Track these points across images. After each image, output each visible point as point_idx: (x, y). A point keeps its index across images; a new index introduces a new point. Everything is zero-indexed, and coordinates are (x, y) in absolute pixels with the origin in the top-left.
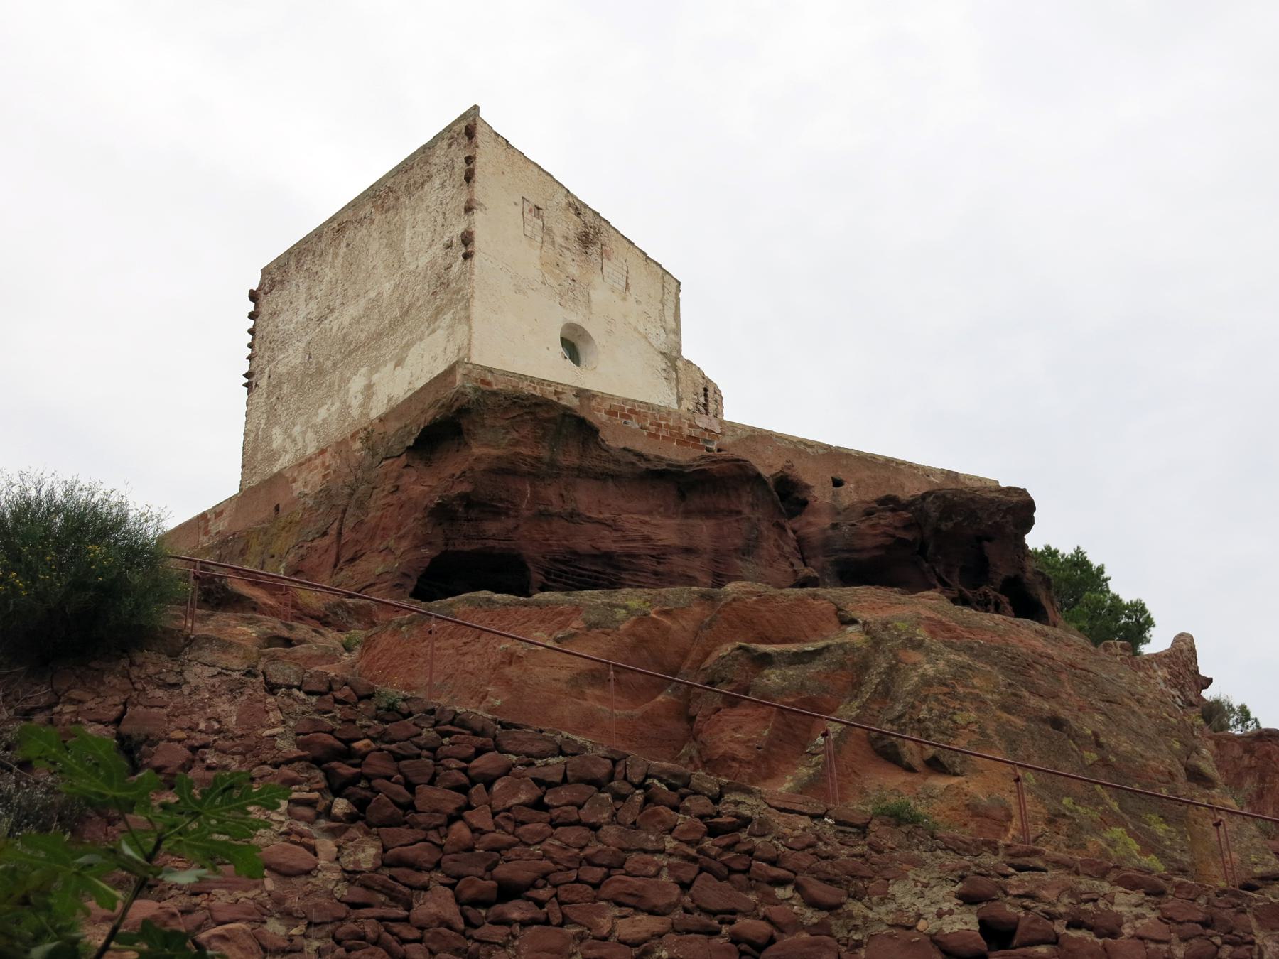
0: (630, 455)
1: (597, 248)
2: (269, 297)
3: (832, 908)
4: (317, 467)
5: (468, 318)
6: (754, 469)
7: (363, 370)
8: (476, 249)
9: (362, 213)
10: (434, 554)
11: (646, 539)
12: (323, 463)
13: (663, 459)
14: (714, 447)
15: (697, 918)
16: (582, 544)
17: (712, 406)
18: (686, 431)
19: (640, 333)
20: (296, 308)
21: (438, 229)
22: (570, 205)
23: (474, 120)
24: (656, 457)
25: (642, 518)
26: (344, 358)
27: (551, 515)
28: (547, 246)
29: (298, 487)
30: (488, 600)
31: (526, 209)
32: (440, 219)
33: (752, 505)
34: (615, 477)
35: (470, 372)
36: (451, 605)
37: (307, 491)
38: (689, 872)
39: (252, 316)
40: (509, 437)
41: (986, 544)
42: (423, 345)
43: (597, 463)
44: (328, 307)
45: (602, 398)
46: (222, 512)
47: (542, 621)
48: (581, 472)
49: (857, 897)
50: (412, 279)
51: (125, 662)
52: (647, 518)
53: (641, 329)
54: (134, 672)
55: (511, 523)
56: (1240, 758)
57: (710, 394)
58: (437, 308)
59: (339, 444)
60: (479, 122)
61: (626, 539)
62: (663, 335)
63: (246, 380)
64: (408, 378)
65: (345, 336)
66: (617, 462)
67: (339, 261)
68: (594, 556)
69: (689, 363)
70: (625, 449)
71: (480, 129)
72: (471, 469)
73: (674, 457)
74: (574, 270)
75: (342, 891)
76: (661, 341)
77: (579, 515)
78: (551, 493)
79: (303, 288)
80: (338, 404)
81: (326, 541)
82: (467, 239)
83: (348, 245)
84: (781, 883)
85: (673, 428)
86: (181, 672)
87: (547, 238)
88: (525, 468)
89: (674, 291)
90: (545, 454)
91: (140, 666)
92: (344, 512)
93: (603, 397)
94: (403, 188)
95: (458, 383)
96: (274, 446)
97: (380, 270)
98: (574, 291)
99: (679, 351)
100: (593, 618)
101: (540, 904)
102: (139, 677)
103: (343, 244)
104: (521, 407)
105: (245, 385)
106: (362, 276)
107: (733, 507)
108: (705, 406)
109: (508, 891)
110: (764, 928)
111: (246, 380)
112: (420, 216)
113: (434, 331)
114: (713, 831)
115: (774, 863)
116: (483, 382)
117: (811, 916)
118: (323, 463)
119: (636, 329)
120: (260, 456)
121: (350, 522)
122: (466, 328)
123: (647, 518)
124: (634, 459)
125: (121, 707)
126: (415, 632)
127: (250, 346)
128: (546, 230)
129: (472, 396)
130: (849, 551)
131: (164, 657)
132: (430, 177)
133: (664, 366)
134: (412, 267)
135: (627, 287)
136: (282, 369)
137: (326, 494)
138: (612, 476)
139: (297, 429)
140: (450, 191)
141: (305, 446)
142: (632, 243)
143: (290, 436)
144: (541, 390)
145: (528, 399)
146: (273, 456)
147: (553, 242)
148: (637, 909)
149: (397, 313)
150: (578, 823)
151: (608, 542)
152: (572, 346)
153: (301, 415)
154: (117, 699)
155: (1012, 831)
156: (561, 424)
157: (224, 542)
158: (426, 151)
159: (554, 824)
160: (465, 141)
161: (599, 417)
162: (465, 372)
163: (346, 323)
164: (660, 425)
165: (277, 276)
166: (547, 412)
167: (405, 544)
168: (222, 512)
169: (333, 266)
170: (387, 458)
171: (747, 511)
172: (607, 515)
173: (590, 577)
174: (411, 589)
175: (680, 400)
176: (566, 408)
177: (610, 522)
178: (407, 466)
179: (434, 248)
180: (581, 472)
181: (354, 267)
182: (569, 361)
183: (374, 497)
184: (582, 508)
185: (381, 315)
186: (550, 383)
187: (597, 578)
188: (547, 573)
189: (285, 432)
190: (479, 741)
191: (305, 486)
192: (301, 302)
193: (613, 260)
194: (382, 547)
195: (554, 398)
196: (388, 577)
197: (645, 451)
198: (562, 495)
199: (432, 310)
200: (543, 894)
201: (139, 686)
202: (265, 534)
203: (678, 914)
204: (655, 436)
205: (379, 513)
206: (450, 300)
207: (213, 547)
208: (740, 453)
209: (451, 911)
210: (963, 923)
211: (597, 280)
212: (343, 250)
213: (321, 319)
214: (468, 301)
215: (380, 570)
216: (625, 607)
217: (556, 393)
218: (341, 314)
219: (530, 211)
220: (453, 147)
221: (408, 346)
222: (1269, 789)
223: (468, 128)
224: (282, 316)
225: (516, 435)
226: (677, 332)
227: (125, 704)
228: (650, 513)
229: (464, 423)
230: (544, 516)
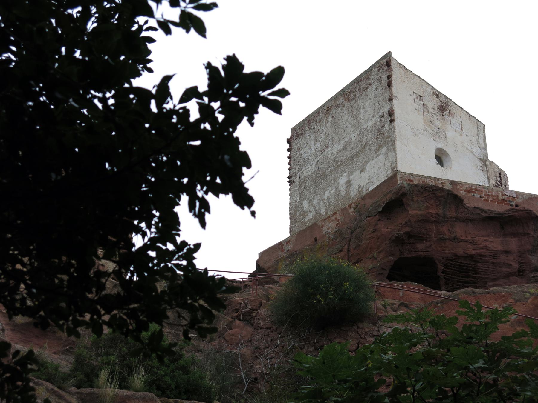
0: (477, 210)
1: (447, 112)
2: (296, 141)
4: (333, 220)
5: (395, 149)
6: (534, 214)
7: (345, 174)
8: (395, 118)
9: (338, 102)
10: (395, 259)
11: (487, 248)
12: (336, 218)
13: (492, 211)
14: (514, 204)
17: (503, 181)
18: (501, 197)
19: (469, 150)
20: (310, 146)
21: (377, 108)
22: (434, 93)
23: (390, 58)
24: (489, 210)
25: (485, 238)
26: (336, 168)
27: (445, 239)
28: (426, 113)
29: (325, 229)
30: (473, 292)
31: (415, 98)
32: (377, 104)
33: (534, 230)
34: (471, 220)
35: (403, 176)
36: (458, 294)
37: (329, 231)
39: (289, 150)
40: (425, 205)
42: (373, 162)
44: (325, 145)
45: (462, 185)
46: (289, 242)
47: (496, 300)
48: (457, 219)
50: (366, 132)
51: (355, 327)
52: (487, 239)
53: (470, 148)
54: (360, 331)
55: (428, 244)
57: (502, 176)
58: (379, 145)
59: (343, 210)
60: (392, 59)
61: (479, 248)
62: (479, 150)
63: (289, 180)
64: (367, 177)
65: (335, 159)
66: (472, 213)
67: (329, 125)
68: (465, 257)
69: (491, 163)
70: (475, 207)
71: (392, 62)
72: (410, 221)
73: (497, 210)
74: (438, 123)
76: (478, 153)
77: (457, 239)
78: (444, 229)
79: (312, 137)
80: (334, 190)
81: (343, 254)
82: (391, 113)
83: (333, 117)
85: (495, 196)
86: (379, 331)
87: (425, 110)
88: (432, 219)
89: (482, 129)
90: (441, 212)
91: (362, 328)
92: (350, 241)
93: (463, 184)
94: (357, 90)
95: (399, 182)
96: (305, 209)
97: (350, 128)
98: (439, 133)
99: (487, 157)
100: (517, 298)
102: (362, 333)
103: (330, 117)
104: (429, 191)
105: (288, 182)
106: (341, 131)
107: (526, 232)
108: (500, 182)
111: (289, 180)
112: (367, 103)
113: (378, 156)
116: (409, 180)
118: (336, 218)
119: (467, 148)
120: (298, 214)
121: (353, 245)
122: (394, 154)
123: (487, 239)
124: (480, 212)
125: (357, 345)
126: (445, 306)
127: (289, 164)
128: (425, 106)
129: (407, 188)
131: (371, 325)
132: (370, 85)
133: (481, 165)
134: (365, 126)
135: (462, 130)
136: (305, 174)
137: (339, 233)
138: (470, 220)
139: (315, 202)
140: (380, 91)
141: (320, 209)
142: (462, 109)
143: (312, 205)
144: (435, 182)
145: (431, 188)
146: (304, 214)
147: (428, 111)
149: (359, 147)
151: (471, 250)
152: (440, 158)
153: (317, 195)
154: (355, 342)
156: (445, 197)
157: (292, 255)
158: (367, 73)
160: (386, 68)
161: (462, 193)
162: (401, 176)
163: (335, 153)
164: (489, 195)
165: (299, 131)
166: (441, 193)
167: (382, 255)
168: (289, 242)
169: (326, 127)
170: (369, 217)
171: (532, 233)
172: (469, 238)
173: (463, 266)
174: (386, 275)
175: (489, 180)
176: (448, 191)
177: (471, 241)
178: (379, 220)
179: (375, 118)
180: (457, 219)
181: (336, 127)
182: (439, 165)
183: (364, 234)
185: (352, 148)
186: (438, 179)
187: (466, 267)
188: (445, 265)
189: (310, 203)
191: (328, 229)
192: (312, 143)
193: (455, 117)
194: (370, 256)
195: (441, 186)
196: (375, 270)
197: (483, 208)
198: (449, 230)
199: (376, 146)
201: (363, 336)
202: (311, 251)
204: (487, 201)
205: (368, 242)
206: (385, 141)
207: (287, 257)
208: (527, 207)
211: (448, 127)
212: (330, 119)
213: (322, 151)
214: (394, 142)
215: (370, 267)
216: (529, 292)
217: (442, 183)
218: (332, 149)
219: (417, 98)
220: (380, 71)
221: (366, 162)
223: (386, 62)
224: (304, 150)
225: (428, 204)
226: (485, 148)
227: (358, 344)
228: (488, 236)
229: (404, 200)
230: (443, 240)
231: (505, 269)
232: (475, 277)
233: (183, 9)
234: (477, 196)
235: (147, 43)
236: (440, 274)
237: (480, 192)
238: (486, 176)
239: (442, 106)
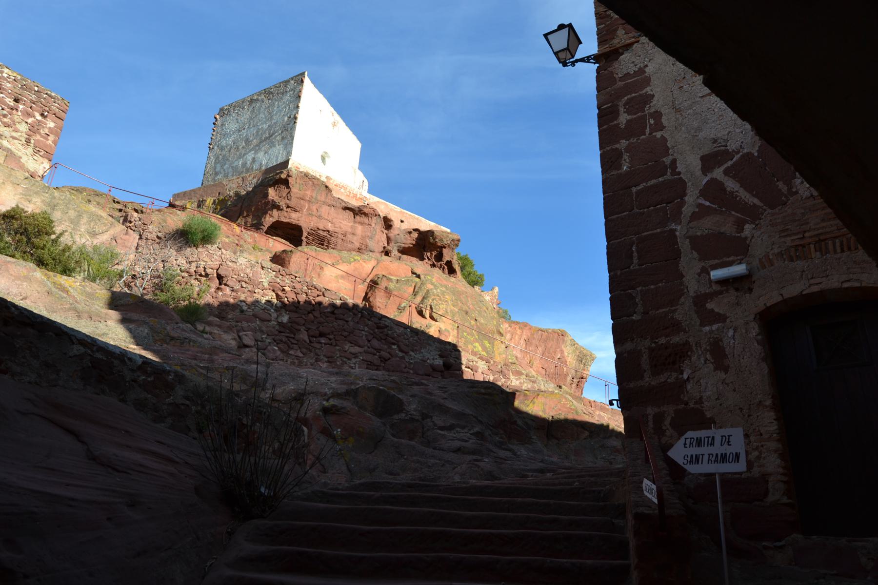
3: (406, 353)
11: (340, 227)
15: (371, 350)
16: (321, 227)
38: (370, 338)
48: (324, 203)
49: (413, 351)
75: (277, 327)
84: (394, 344)
101: (330, 339)
109: (322, 335)
110: (388, 356)
114: (378, 328)
115: (393, 338)
117: (401, 354)
130: (781, 547)
148: (356, 345)
150: (343, 319)
151: (329, 227)
159: (336, 319)
171: (373, 225)
184: (323, 215)
190: (318, 293)
200: (331, 337)
203: (366, 348)
208: (374, 207)
209: (306, 338)
210: (439, 362)
231: (349, 246)
233: (386, 231)
234: (342, 190)
236: (303, 238)
237: (345, 189)
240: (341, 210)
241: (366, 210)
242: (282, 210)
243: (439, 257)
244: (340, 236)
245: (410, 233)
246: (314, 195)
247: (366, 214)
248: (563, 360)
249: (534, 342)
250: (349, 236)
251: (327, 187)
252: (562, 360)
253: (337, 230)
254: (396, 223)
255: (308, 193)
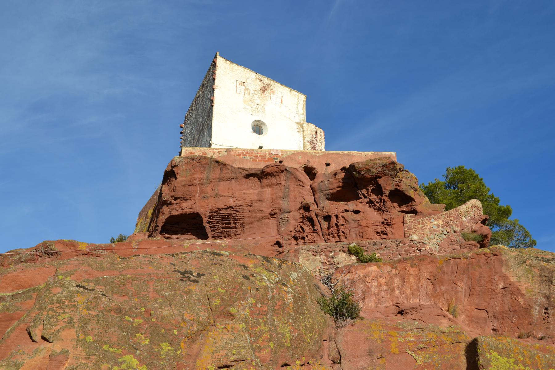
1: (269, 91)
10: (166, 217)
11: (244, 199)
16: (221, 205)
41: (378, 180)
43: (226, 175)
48: (220, 179)
55: (193, 202)
56: (391, 271)
74: (258, 101)
87: (246, 92)
88: (197, 182)
123: (246, 192)
124: (241, 171)
151: (231, 202)
152: (258, 128)
155: (67, 365)
171: (283, 183)
188: (209, 217)
204: (256, 161)
222: (407, 282)
231: (259, 215)
232: (235, 223)
234: (247, 157)
235: (220, 61)
236: (205, 224)
238: (302, 135)
239: (264, 87)
240: (244, 180)
241: (268, 170)
242: (170, 204)
243: (378, 191)
244: (245, 208)
245: (335, 174)
246: (204, 175)
247: (271, 175)
248: (511, 288)
249: (446, 277)
250: (257, 205)
251: (217, 162)
252: (511, 290)
253: (240, 203)
254: (321, 170)
255: (197, 176)
